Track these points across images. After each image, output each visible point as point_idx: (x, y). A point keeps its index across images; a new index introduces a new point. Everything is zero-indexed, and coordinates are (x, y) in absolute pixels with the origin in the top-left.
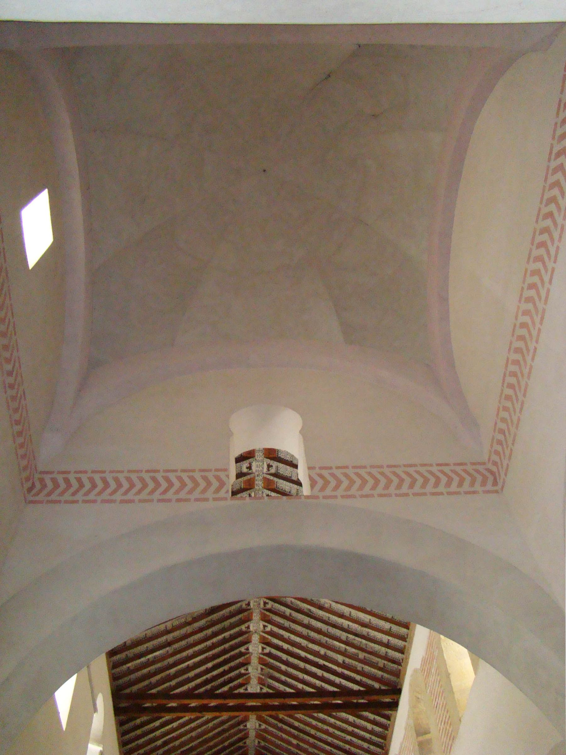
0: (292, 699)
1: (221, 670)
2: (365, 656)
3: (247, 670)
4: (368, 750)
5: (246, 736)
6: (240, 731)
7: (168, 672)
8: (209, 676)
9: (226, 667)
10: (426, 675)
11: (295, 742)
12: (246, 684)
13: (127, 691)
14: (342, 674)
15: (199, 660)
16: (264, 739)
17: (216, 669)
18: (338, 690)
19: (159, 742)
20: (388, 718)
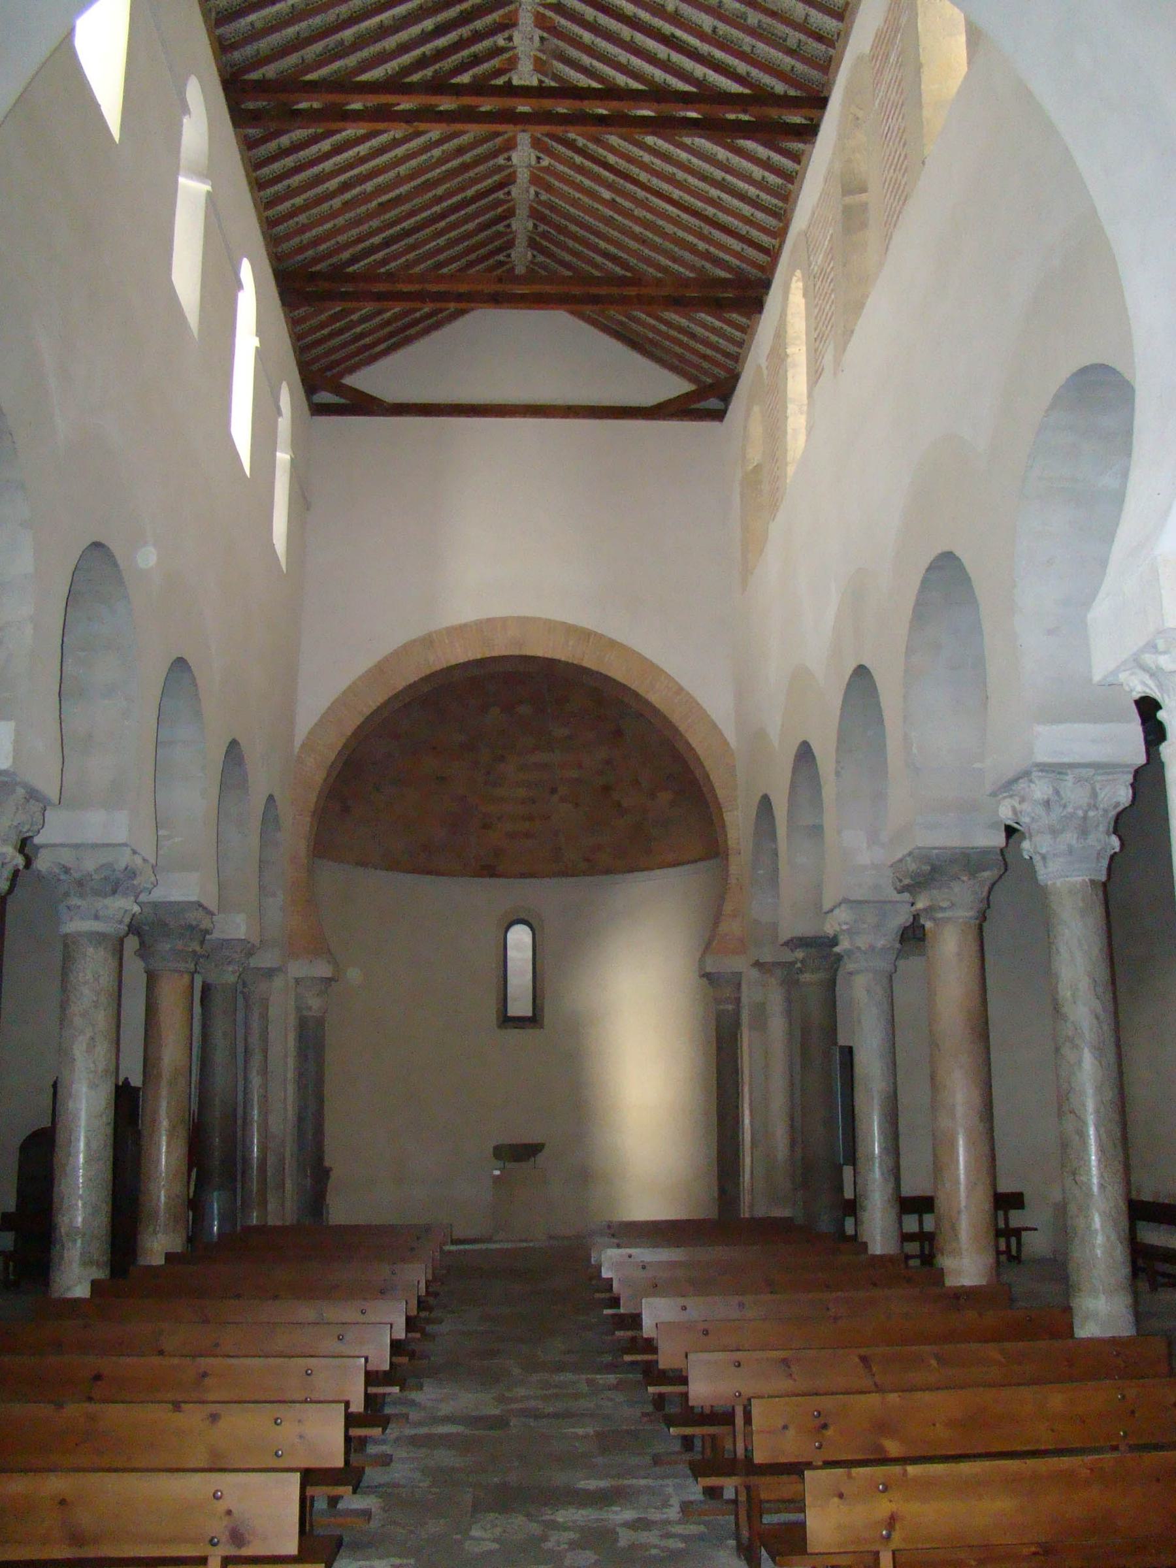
0: (598, 103)
1: (452, 37)
2: (760, 21)
3: (510, 39)
4: (751, 220)
5: (510, 180)
6: (500, 169)
7: (338, 37)
8: (428, 48)
9: (465, 31)
10: (878, 70)
11: (607, 195)
12: (510, 70)
13: (255, 76)
14: (709, 58)
15: (404, 13)
16: (549, 188)
17: (444, 35)
18: (694, 90)
19: (333, 184)
20: (796, 158)
